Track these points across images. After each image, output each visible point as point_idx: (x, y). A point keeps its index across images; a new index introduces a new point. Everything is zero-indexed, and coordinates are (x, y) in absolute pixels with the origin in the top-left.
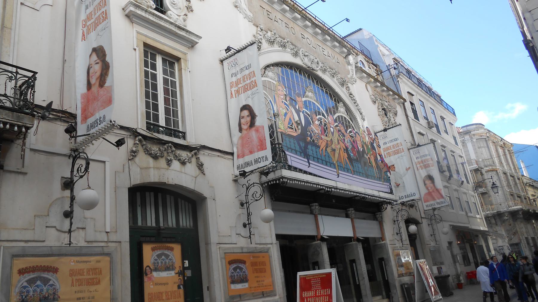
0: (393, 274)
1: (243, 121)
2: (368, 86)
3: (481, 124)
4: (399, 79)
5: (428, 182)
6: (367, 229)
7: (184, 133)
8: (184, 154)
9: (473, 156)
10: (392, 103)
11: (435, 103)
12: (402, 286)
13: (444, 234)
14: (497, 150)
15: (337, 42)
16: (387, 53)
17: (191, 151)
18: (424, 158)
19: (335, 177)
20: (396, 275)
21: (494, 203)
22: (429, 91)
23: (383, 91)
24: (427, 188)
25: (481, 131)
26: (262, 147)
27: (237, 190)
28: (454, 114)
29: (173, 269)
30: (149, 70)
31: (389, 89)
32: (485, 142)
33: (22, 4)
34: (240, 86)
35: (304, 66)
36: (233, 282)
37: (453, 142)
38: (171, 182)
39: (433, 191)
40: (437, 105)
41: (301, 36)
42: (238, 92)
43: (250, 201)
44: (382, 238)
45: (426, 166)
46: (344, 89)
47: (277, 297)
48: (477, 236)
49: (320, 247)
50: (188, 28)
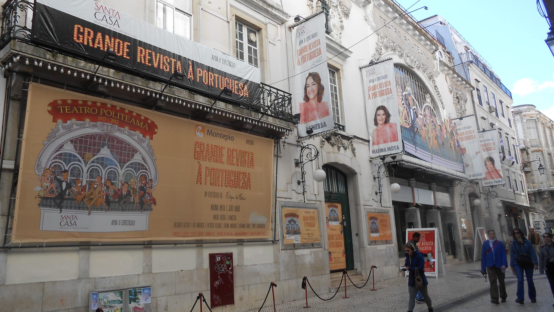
0: (459, 236)
1: (378, 118)
2: (447, 77)
3: (533, 105)
4: (469, 68)
5: (489, 163)
6: (443, 199)
7: (344, 127)
8: (345, 141)
9: (521, 136)
10: (463, 91)
11: (496, 88)
12: (465, 246)
13: (497, 207)
14: (545, 132)
15: (390, 7)
16: (459, 40)
17: (349, 140)
18: (487, 142)
19: (430, 160)
20: (461, 238)
21: (536, 182)
22: (492, 76)
23: (458, 81)
24: (487, 168)
25: (533, 112)
26: (395, 139)
27: (372, 168)
28: (511, 98)
29: (338, 221)
30: (238, 40)
31: (459, 76)
32: (534, 123)
33: (202, 9)
34: (377, 90)
35: (406, 65)
36: (372, 232)
37: (508, 125)
38: (341, 162)
39: (493, 171)
40: (498, 90)
41: (404, 38)
42: (375, 95)
43: (305, 161)
44: (452, 208)
45: (488, 149)
46: (431, 83)
47: (393, 245)
48: (521, 211)
49: (415, 212)
50: (342, 44)
